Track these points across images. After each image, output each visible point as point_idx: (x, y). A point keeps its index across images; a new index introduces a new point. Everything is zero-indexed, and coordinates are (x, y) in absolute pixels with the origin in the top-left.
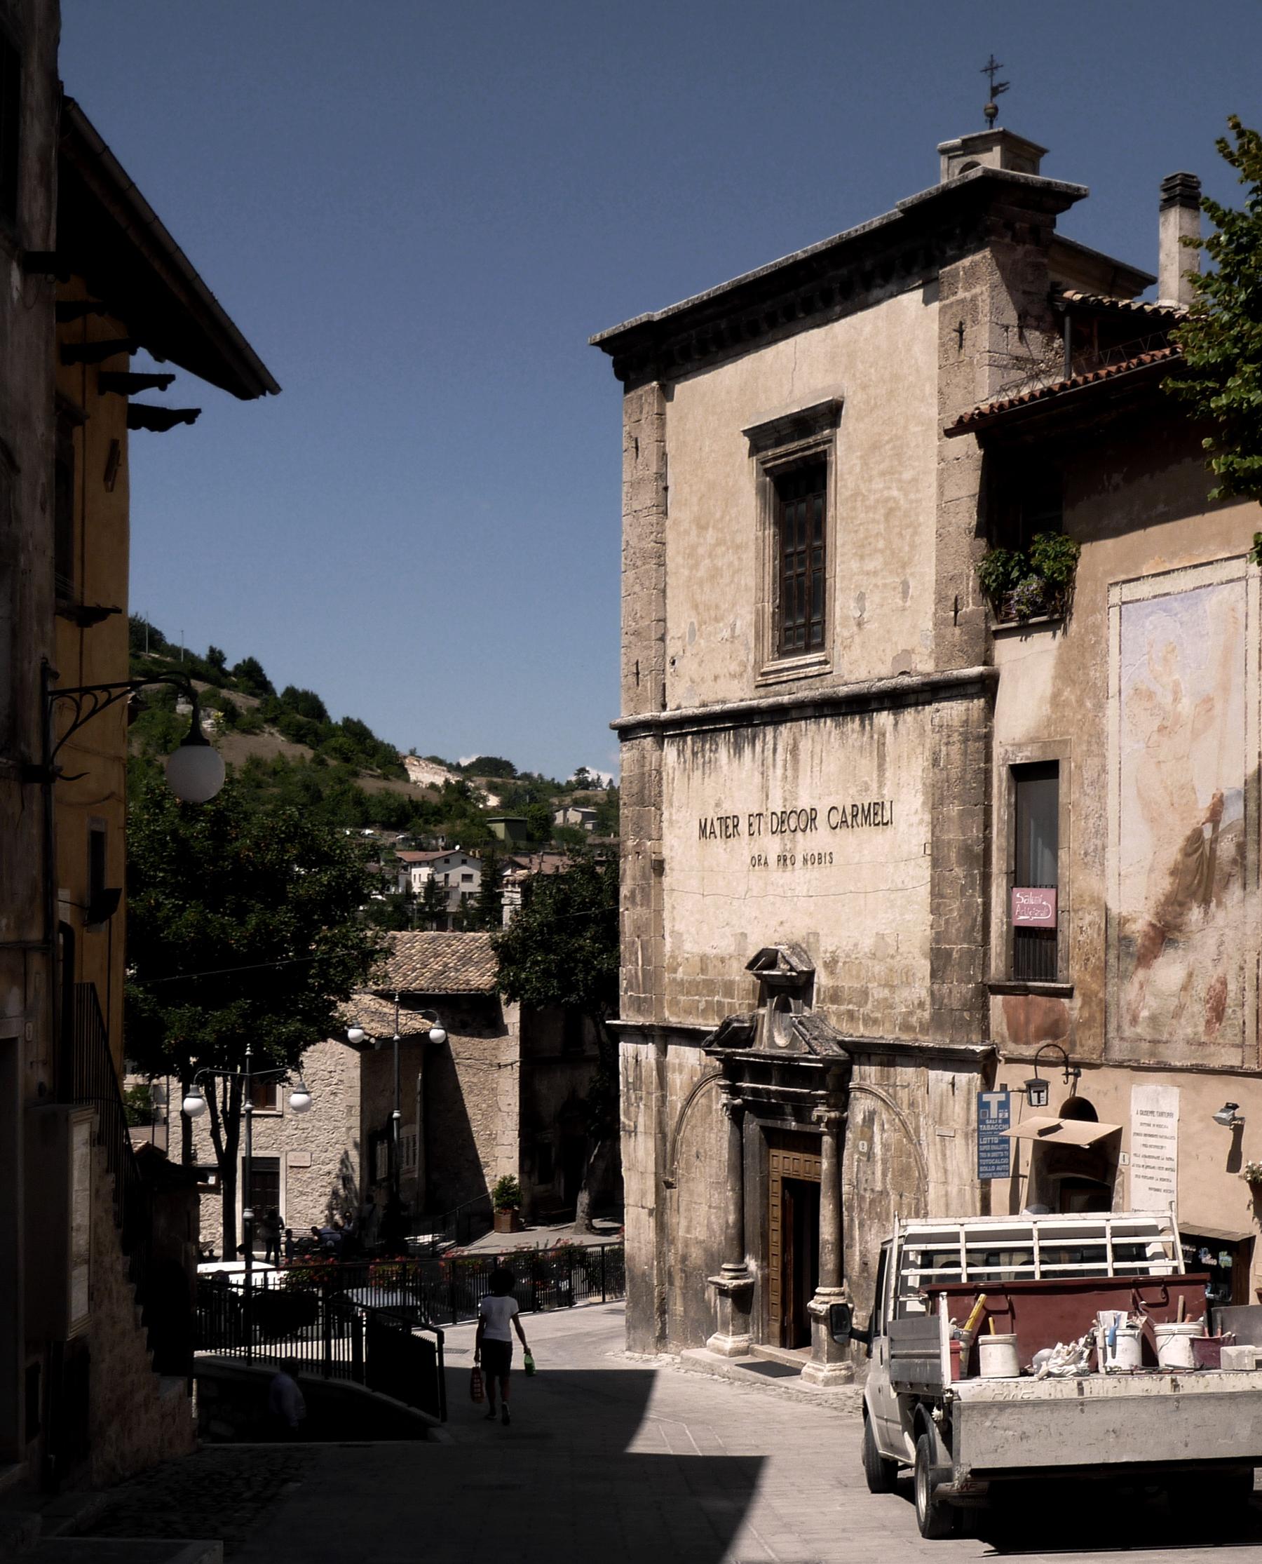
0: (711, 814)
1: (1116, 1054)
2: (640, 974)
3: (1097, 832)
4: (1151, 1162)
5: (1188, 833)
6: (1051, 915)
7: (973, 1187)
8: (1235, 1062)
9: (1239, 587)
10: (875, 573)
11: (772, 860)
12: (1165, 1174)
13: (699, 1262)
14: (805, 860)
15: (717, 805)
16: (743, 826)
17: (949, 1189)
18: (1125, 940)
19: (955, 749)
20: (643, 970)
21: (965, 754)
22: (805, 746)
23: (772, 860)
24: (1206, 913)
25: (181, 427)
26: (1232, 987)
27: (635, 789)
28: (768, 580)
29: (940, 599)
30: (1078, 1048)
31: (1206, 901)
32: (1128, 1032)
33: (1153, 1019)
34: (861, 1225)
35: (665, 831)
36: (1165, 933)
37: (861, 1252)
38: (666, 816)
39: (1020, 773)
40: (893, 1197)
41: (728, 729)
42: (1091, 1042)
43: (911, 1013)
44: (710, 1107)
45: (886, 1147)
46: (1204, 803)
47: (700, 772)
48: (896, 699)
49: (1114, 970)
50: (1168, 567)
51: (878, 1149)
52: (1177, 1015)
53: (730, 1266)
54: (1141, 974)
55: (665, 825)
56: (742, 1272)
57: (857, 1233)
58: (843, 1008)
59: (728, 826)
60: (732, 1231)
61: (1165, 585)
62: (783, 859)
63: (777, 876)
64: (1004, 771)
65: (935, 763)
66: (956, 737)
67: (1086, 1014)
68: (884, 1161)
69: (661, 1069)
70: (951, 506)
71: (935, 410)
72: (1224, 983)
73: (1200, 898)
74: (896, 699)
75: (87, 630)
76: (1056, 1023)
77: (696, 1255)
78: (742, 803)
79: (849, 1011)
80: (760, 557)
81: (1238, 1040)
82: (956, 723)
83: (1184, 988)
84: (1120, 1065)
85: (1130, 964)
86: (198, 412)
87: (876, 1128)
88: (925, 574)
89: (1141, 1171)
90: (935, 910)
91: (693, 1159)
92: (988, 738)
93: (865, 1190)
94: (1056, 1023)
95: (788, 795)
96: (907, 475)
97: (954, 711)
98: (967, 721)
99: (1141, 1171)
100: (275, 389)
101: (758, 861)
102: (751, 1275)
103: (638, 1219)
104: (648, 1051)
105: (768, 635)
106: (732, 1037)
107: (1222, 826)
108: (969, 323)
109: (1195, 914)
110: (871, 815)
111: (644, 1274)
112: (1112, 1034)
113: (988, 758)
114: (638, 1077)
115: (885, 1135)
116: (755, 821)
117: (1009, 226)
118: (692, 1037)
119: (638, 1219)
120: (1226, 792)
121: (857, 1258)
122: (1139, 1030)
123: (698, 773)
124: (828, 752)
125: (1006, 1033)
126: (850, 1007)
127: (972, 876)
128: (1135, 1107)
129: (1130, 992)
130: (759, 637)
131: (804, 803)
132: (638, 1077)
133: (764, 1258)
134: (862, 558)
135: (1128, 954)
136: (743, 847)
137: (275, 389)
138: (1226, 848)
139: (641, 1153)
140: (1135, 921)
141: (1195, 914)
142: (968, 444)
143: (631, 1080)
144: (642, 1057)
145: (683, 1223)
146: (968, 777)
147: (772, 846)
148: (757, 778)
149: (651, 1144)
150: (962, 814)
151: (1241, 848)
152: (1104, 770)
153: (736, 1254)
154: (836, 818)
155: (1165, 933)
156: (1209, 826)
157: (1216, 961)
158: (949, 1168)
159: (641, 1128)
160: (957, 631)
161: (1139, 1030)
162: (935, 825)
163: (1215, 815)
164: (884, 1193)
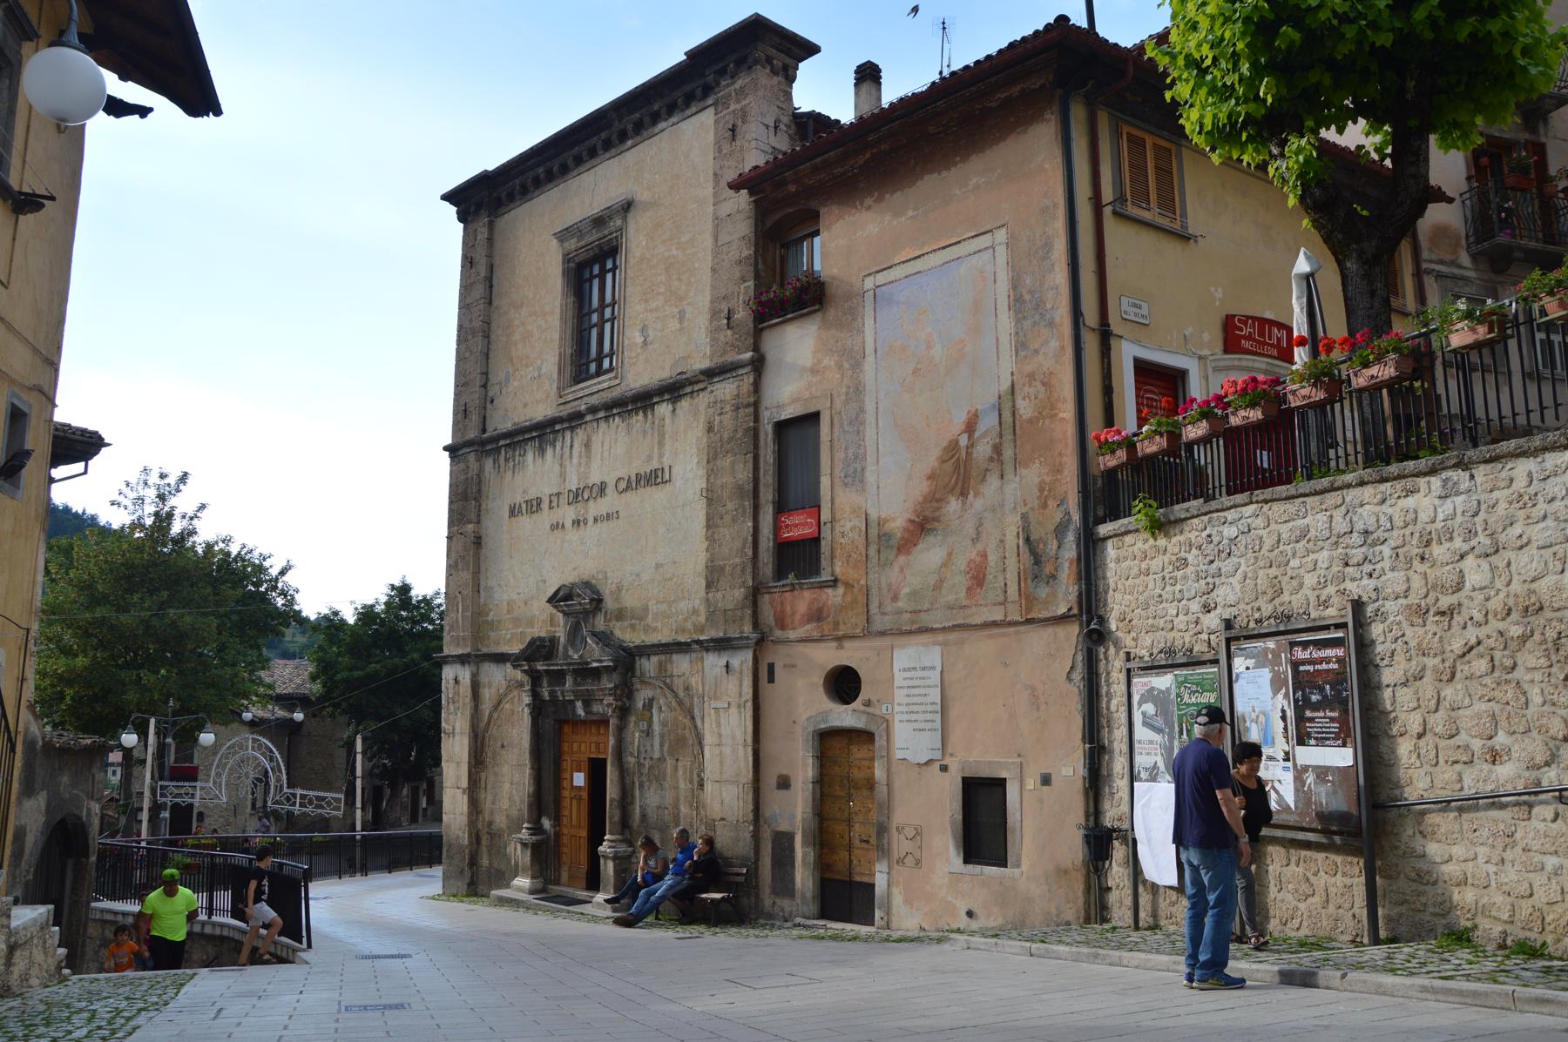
1: (879, 623)
3: (856, 458)
4: (915, 708)
5: (945, 444)
6: (815, 528)
7: (745, 745)
8: (999, 617)
9: (987, 255)
10: (657, 310)
11: (568, 524)
12: (929, 716)
14: (596, 520)
15: (525, 492)
16: (545, 505)
18: (885, 537)
19: (727, 418)
21: (737, 418)
22: (597, 440)
23: (568, 524)
24: (964, 503)
25: (135, 119)
26: (992, 558)
29: (714, 314)
30: (842, 627)
31: (964, 494)
32: (889, 608)
33: (914, 594)
34: (641, 786)
36: (923, 525)
39: (782, 427)
41: (533, 438)
42: (853, 620)
43: (686, 620)
45: (664, 724)
46: (960, 419)
48: (673, 390)
49: (875, 561)
50: (918, 253)
51: (656, 727)
52: (938, 587)
54: (902, 559)
57: (637, 793)
59: (534, 506)
61: (918, 265)
62: (577, 523)
63: (572, 535)
64: (770, 429)
65: (710, 429)
66: (728, 408)
67: (849, 598)
68: (662, 736)
69: (476, 687)
70: (725, 249)
71: (710, 190)
72: (984, 556)
73: (958, 490)
74: (673, 390)
75: (21, 217)
76: (820, 610)
78: (545, 489)
80: (563, 320)
81: (1001, 598)
82: (728, 397)
83: (945, 565)
84: (883, 634)
85: (891, 554)
86: (151, 110)
87: (655, 711)
88: (700, 302)
89: (905, 717)
90: (711, 539)
92: (756, 405)
94: (820, 610)
96: (684, 239)
97: (726, 389)
98: (738, 396)
99: (905, 717)
100: (218, 112)
101: (557, 526)
103: (454, 797)
104: (465, 674)
105: (568, 368)
106: (540, 649)
107: (977, 434)
109: (953, 505)
110: (654, 478)
112: (874, 609)
113: (757, 419)
114: (457, 693)
116: (555, 499)
117: (769, 60)
118: (500, 658)
119: (454, 797)
120: (979, 407)
121: (638, 812)
122: (900, 604)
123: (509, 473)
128: (897, 665)
129: (893, 574)
131: (595, 479)
132: (457, 693)
133: (557, 819)
134: (646, 301)
135: (889, 547)
136: (546, 517)
137: (218, 112)
138: (983, 450)
139: (457, 749)
140: (894, 520)
141: (953, 505)
142: (743, 198)
144: (460, 678)
145: (490, 798)
146: (739, 435)
147: (568, 513)
148: (557, 468)
149: (466, 741)
150: (733, 463)
151: (997, 449)
152: (862, 410)
154: (623, 485)
155: (923, 525)
156: (965, 436)
157: (975, 541)
159: (458, 730)
160: (729, 332)
161: (900, 604)
162: (711, 473)
163: (970, 428)
164: (662, 760)
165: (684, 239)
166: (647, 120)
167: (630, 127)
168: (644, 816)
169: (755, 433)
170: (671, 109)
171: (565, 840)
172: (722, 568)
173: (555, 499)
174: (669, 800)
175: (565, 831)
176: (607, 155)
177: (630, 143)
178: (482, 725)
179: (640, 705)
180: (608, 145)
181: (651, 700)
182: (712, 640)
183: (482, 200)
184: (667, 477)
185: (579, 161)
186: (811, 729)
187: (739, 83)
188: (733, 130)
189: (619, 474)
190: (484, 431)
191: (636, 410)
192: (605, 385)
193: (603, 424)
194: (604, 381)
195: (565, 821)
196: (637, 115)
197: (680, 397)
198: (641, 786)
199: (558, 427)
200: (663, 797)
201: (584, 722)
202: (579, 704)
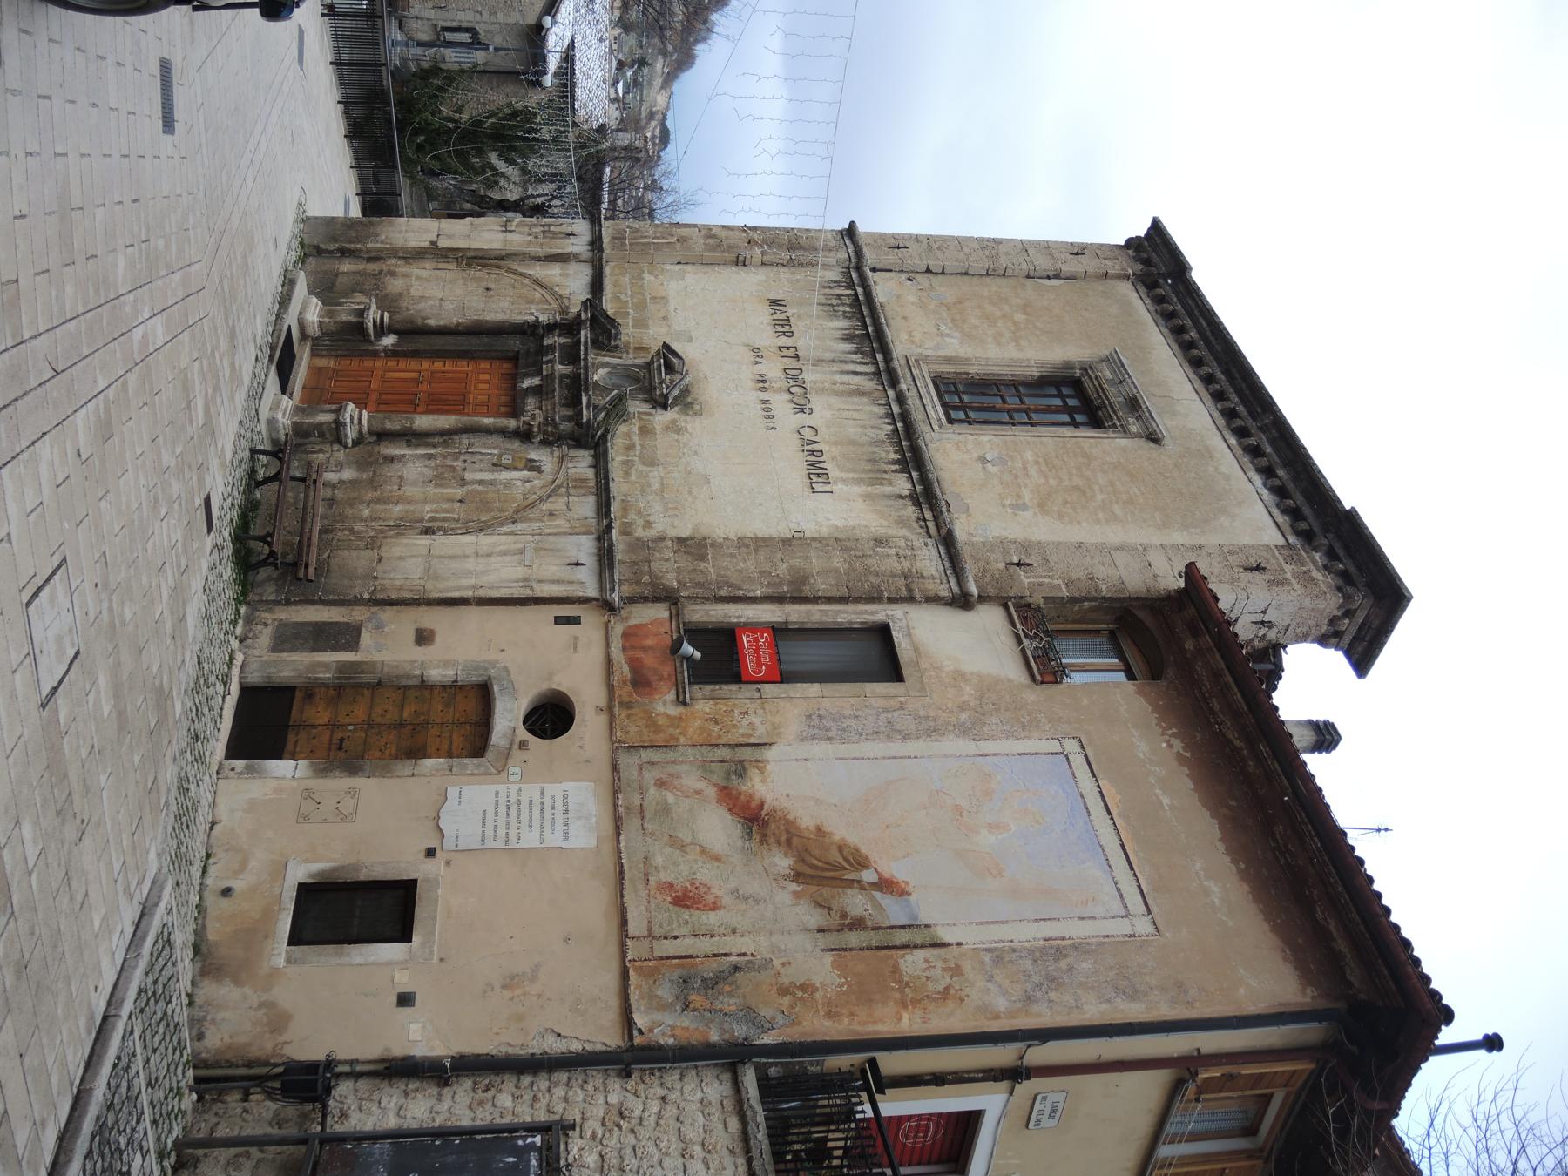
17: (472, 560)
23: (760, 369)
28: (996, 370)
40: (459, 492)
44: (532, 302)
45: (508, 484)
51: (505, 475)
56: (381, 331)
68: (492, 483)
77: (394, 286)
87: (526, 473)
91: (484, 284)
103: (428, 231)
108: (1266, 577)
111: (377, 235)
115: (519, 483)
119: (428, 231)
125: (632, 622)
127: (780, 584)
130: (948, 359)
133: (393, 353)
136: (767, 339)
145: (425, 274)
146: (872, 579)
148: (828, 356)
150: (836, 571)
158: (493, 559)
159: (509, 236)
160: (1001, 565)
164: (463, 482)
165: (1117, 509)
166: (1264, 462)
167: (1253, 441)
168: (391, 460)
169: (874, 598)
170: (1280, 492)
171: (368, 363)
172: (702, 558)
173: (791, 352)
174: (409, 491)
175: (379, 364)
176: (1216, 414)
177: (1233, 441)
179: (533, 455)
180: (1229, 415)
181: (538, 470)
182: (611, 545)
183: (1156, 263)
184: (818, 487)
185: (1208, 380)
186: (493, 672)
187: (1318, 575)
188: (1258, 568)
190: (874, 270)
191: (901, 451)
192: (932, 413)
193: (881, 411)
194: (936, 412)
195: (392, 363)
196: (1269, 450)
197: (917, 504)
198: (430, 457)
199: (879, 357)
200: (414, 483)
202: (537, 381)
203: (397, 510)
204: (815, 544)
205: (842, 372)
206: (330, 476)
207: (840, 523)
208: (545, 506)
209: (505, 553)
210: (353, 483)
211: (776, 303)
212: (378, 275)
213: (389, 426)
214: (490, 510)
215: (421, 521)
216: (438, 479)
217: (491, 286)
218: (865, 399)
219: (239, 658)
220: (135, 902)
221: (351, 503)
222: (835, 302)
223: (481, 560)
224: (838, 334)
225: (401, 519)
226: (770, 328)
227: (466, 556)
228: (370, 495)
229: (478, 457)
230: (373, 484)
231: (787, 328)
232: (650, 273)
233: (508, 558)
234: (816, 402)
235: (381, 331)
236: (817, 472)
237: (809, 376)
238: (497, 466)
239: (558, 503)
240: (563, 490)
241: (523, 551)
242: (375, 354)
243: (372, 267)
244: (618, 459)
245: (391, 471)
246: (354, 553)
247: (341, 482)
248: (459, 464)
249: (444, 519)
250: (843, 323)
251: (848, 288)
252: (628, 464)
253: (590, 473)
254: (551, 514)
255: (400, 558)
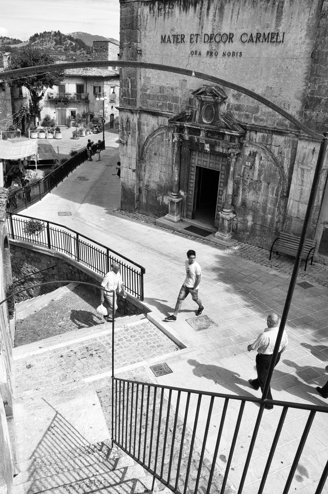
0: (168, 33)
2: (130, 91)
13: (154, 188)
14: (224, 54)
17: (304, 188)
20: (131, 90)
23: (204, 52)
27: (128, 23)
34: (244, 190)
35: (142, 39)
37: (242, 199)
38: (143, 33)
40: (264, 184)
44: (163, 140)
45: (261, 165)
47: (162, 17)
53: (175, 194)
55: (142, 37)
56: (179, 196)
58: (242, 113)
60: (176, 183)
62: (210, 54)
68: (260, 171)
79: (246, 115)
93: (247, 179)
95: (215, 27)
102: (182, 196)
111: (130, 189)
115: (262, 162)
124: (243, 10)
126: (247, 113)
133: (187, 191)
143: (124, 127)
145: (147, 175)
148: (197, 20)
153: (177, 190)
159: (129, 143)
172: (319, 100)
174: (261, 199)
178: (143, 143)
179: (247, 153)
184: (280, 38)
189: (244, 31)
201: (206, 152)
203: (269, 205)
204: (319, 48)
205: (208, 15)
206: (250, 224)
207: (304, 32)
208: (276, 154)
209: (303, 176)
210: (254, 217)
211: (163, 40)
212: (148, 191)
213: (230, 203)
214: (275, 174)
215: (277, 199)
216: (257, 190)
217: (153, 153)
218: (226, 7)
219: (152, 334)
220: (227, 104)
221: (264, 220)
222: (163, 12)
223: (305, 184)
224: (184, 13)
225: (275, 205)
226: (179, 45)
227: (302, 189)
228: (261, 213)
229: (246, 173)
230: (255, 211)
231: (179, 37)
232: (146, 91)
233: (305, 175)
234: (226, 30)
235: (179, 196)
236: (273, 38)
237: (208, 30)
238: (252, 167)
239: (276, 150)
240: (268, 146)
241: (303, 170)
242: (187, 197)
243: (144, 192)
244: (253, 122)
245: (249, 204)
246: (293, 225)
247: (253, 221)
248: (249, 181)
249: (277, 191)
250: (176, 10)
251: (154, 4)
252: (256, 119)
253: (260, 134)
254: (281, 153)
255: (298, 211)
